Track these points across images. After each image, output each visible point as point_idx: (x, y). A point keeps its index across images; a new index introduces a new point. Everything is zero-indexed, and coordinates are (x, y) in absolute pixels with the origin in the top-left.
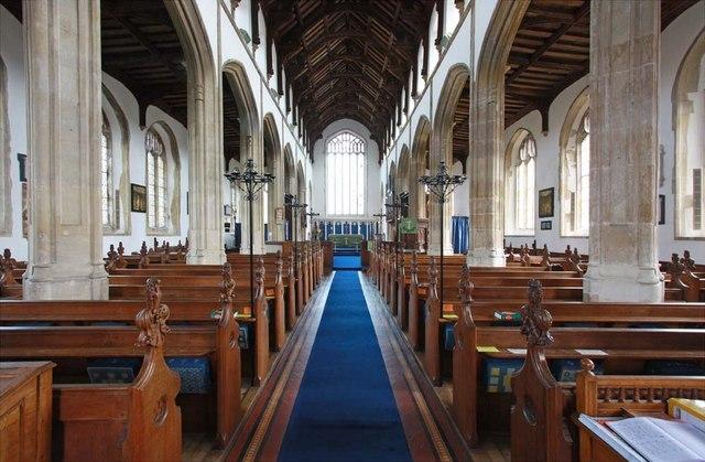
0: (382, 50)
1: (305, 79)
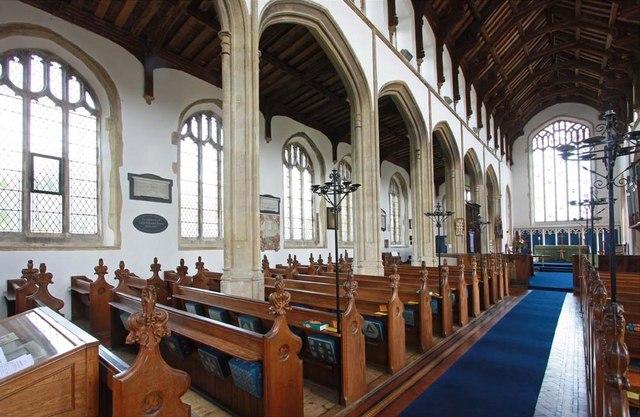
1: (492, 75)
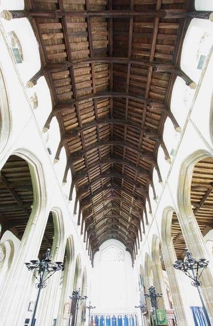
0: (129, 205)
1: (92, 218)
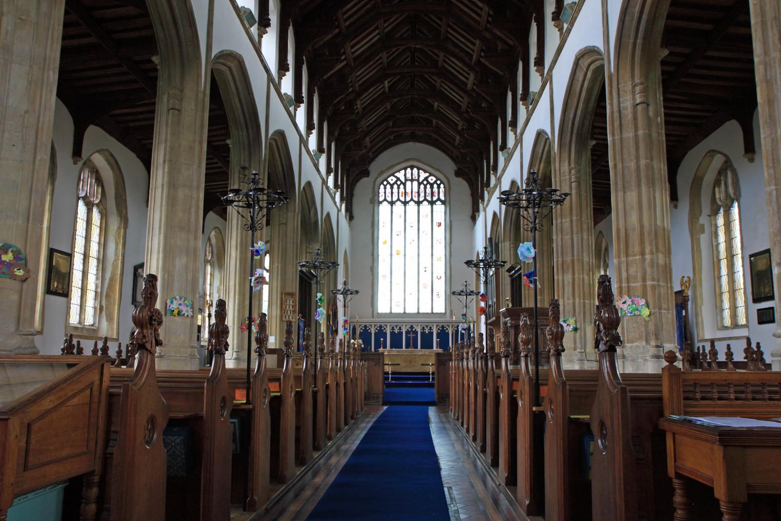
1: (342, 76)
